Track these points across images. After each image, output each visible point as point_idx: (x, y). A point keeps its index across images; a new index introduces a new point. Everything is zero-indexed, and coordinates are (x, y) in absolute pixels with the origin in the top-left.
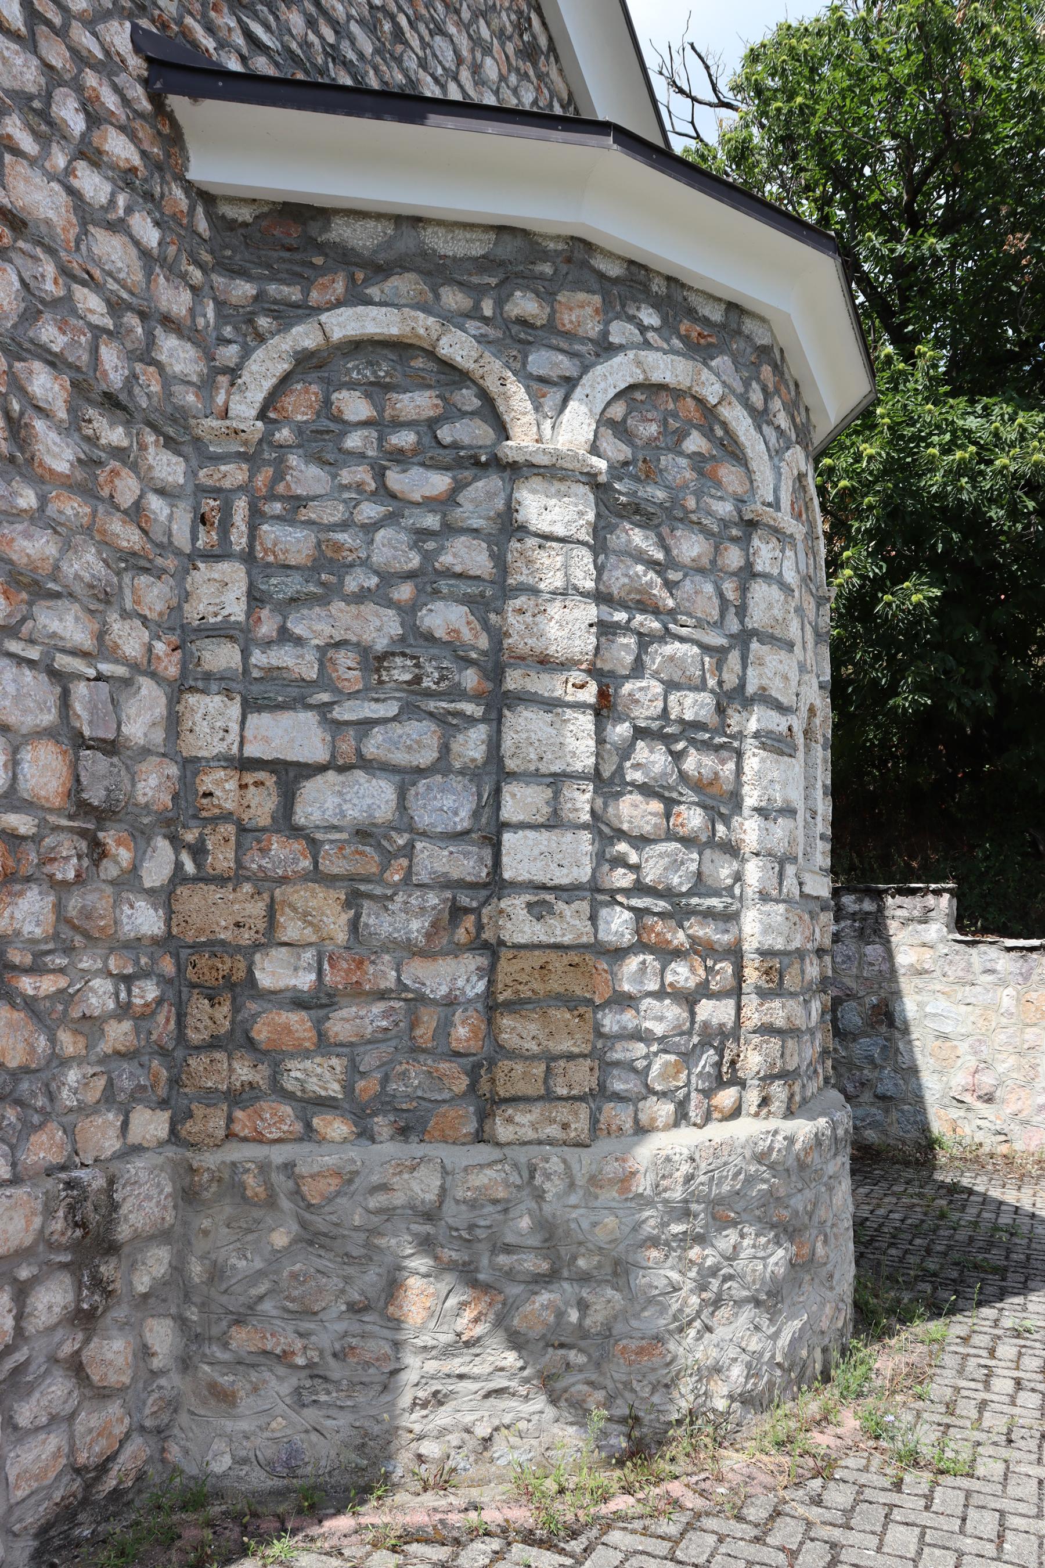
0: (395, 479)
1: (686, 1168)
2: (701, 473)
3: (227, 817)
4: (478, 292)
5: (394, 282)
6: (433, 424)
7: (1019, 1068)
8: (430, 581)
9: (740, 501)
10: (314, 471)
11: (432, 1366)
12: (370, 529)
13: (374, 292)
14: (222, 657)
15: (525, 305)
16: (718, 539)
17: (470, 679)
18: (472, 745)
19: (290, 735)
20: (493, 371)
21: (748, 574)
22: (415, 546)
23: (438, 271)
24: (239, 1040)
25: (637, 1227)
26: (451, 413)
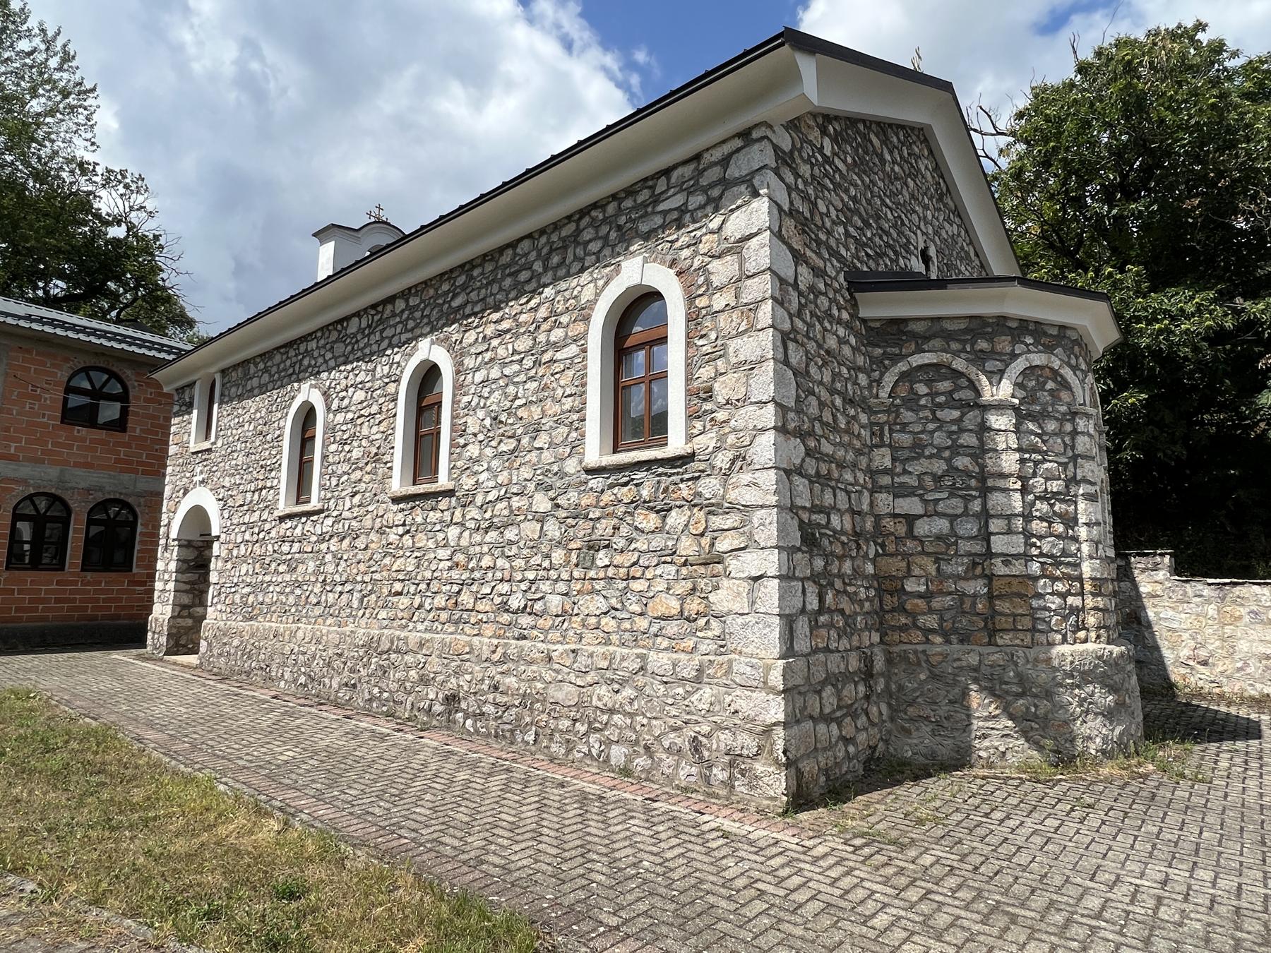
0: (939, 414)
1: (1070, 658)
2: (1052, 396)
3: (892, 534)
4: (964, 342)
5: (932, 342)
6: (951, 393)
7: (1222, 648)
8: (956, 449)
9: (1069, 404)
10: (910, 413)
11: (981, 724)
12: (932, 432)
13: (925, 347)
14: (885, 480)
15: (983, 345)
16: (1061, 421)
17: (973, 483)
18: (976, 506)
19: (911, 505)
20: (973, 371)
21: (1075, 433)
22: (949, 437)
23: (948, 336)
24: (902, 609)
25: (1054, 678)
26: (958, 388)
